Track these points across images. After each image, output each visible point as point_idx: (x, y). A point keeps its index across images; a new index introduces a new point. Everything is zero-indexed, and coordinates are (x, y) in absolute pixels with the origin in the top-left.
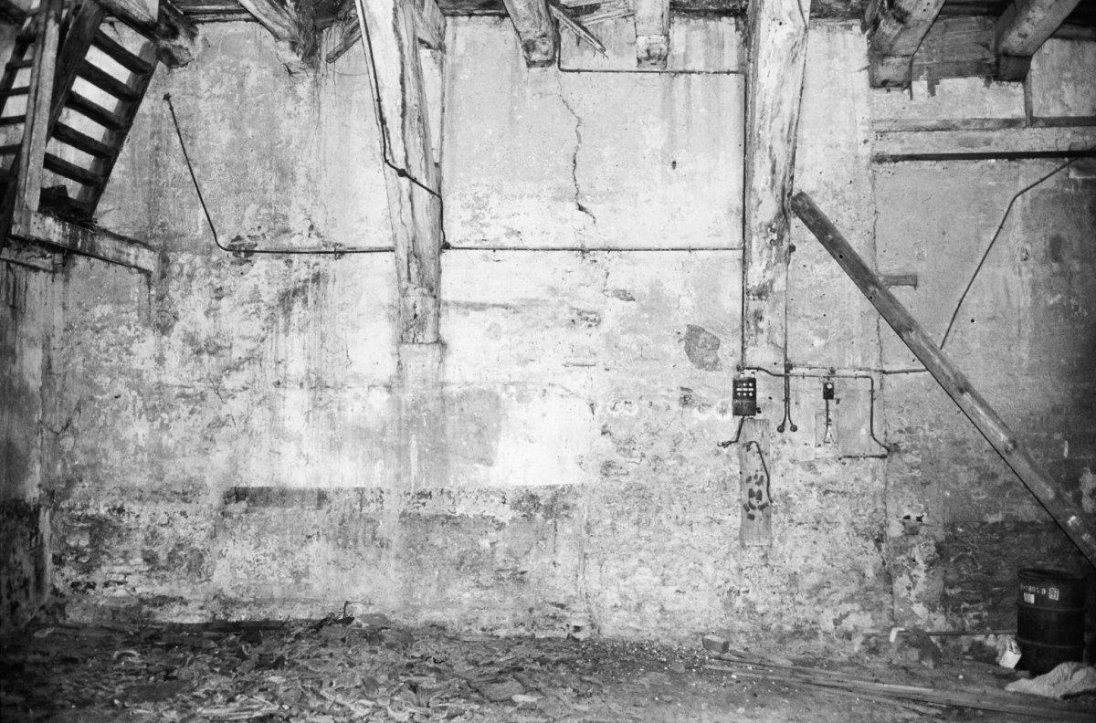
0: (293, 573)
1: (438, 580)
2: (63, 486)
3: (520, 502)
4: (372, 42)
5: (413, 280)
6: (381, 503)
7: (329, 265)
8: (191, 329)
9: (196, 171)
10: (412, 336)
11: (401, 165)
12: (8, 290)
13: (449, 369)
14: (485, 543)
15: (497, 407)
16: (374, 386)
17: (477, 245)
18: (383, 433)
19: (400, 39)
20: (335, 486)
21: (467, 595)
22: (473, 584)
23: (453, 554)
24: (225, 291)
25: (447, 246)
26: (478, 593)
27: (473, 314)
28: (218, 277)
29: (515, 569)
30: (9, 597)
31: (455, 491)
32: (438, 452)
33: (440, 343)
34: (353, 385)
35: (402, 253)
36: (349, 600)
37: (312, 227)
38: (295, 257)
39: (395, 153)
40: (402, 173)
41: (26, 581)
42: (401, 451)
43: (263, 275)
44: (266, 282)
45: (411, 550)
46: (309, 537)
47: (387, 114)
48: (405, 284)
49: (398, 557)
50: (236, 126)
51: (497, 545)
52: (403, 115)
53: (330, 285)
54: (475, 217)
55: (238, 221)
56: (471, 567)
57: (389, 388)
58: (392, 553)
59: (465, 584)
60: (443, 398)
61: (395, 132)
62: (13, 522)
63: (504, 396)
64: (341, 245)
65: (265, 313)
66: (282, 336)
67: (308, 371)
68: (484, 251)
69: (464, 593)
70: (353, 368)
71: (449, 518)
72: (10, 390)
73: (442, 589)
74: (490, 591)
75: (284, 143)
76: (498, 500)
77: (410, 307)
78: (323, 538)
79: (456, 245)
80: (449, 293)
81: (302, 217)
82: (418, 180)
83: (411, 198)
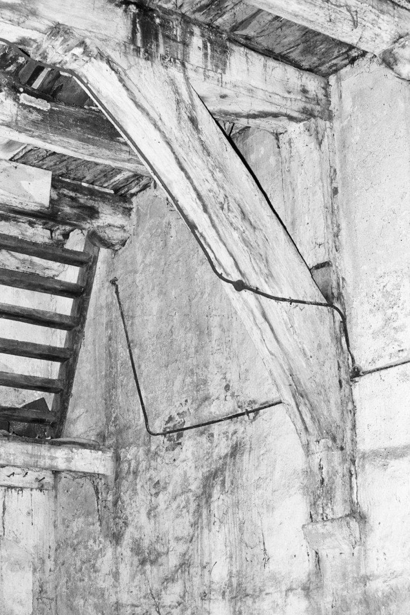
5: (310, 430)
7: (245, 429)
8: (137, 536)
9: (136, 351)
10: (321, 511)
11: (236, 277)
13: (372, 555)
16: (290, 589)
19: (148, 114)
24: (162, 484)
25: (356, 373)
28: (155, 469)
33: (356, 514)
34: (271, 590)
35: (288, 398)
37: (227, 388)
38: (215, 429)
40: (240, 286)
44: (193, 467)
47: (192, 217)
48: (304, 437)
50: (163, 293)
52: (205, 210)
53: (246, 457)
54: (388, 320)
57: (307, 590)
64: (254, 402)
65: (193, 506)
67: (230, 575)
70: (272, 566)
75: (199, 295)
77: (316, 469)
81: (220, 376)
82: (261, 290)
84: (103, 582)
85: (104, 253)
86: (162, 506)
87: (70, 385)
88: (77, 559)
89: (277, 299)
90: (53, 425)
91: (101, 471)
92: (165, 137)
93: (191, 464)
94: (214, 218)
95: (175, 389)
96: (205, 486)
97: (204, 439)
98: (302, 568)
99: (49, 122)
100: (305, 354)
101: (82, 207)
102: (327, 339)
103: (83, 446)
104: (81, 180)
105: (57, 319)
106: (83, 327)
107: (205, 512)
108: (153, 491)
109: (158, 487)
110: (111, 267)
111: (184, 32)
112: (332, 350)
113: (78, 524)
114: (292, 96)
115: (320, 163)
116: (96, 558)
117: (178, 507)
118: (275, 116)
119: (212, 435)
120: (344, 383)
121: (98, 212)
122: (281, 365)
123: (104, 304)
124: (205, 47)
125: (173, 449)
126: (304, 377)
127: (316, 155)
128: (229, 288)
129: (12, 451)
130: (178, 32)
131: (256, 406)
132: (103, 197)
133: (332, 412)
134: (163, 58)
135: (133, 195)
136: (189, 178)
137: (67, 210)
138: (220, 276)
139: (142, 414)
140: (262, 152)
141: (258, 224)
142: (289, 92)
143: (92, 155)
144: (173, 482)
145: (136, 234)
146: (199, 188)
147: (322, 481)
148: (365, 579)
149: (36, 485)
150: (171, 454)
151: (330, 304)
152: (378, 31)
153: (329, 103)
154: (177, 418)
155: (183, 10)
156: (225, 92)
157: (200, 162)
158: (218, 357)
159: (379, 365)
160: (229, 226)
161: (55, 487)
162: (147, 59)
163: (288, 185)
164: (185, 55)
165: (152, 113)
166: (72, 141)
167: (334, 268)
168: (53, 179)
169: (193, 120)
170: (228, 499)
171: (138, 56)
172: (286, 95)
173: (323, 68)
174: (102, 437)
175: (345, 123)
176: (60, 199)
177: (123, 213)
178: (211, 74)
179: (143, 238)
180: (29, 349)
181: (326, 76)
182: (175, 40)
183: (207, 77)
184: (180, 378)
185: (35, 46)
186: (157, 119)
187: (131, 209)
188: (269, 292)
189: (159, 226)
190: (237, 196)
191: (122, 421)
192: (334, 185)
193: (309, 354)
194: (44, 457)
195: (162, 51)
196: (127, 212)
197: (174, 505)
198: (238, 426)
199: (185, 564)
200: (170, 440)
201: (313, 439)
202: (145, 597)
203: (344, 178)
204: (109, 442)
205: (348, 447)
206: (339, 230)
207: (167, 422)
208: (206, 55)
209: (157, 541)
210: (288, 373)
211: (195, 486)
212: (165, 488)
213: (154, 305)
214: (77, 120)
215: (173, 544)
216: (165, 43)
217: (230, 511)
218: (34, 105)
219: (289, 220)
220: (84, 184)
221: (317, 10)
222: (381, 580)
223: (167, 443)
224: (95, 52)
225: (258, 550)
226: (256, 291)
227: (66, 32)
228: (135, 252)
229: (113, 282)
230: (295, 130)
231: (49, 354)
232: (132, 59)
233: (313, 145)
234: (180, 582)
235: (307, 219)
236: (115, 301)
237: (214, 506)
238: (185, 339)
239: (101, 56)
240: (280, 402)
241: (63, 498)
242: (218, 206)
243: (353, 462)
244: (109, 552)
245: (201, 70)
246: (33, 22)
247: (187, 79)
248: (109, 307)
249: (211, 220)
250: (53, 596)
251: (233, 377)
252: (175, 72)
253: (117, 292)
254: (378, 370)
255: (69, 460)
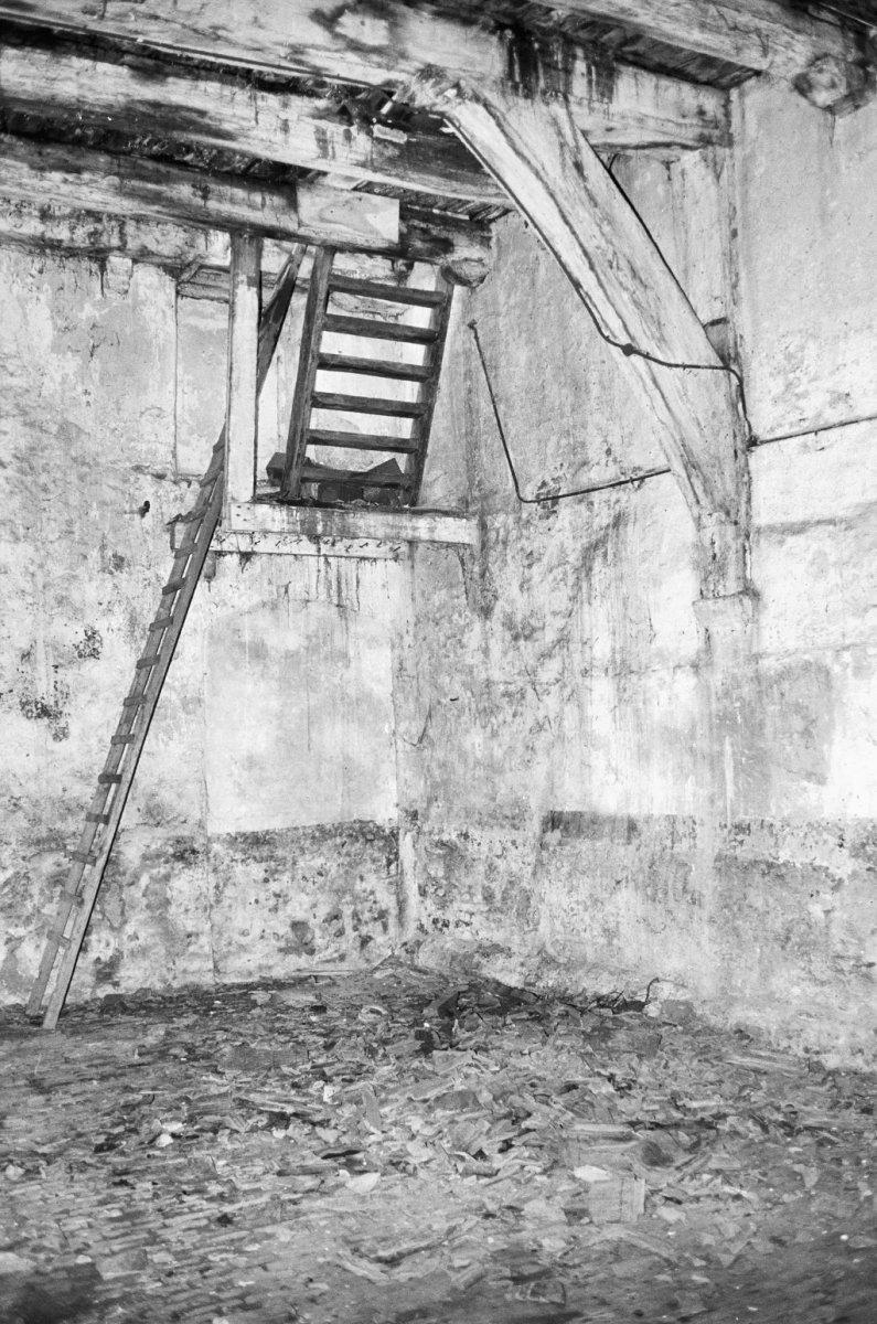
0: (605, 930)
1: (760, 962)
2: (425, 805)
3: (863, 845)
4: (506, 180)
6: (694, 838)
7: (629, 498)
8: (508, 609)
9: (502, 408)
11: (624, 340)
12: (329, 588)
13: (766, 633)
14: (816, 910)
15: (829, 686)
16: (679, 666)
17: (796, 430)
18: (692, 736)
19: (529, 163)
20: (645, 812)
21: (796, 991)
22: (803, 974)
23: (777, 924)
24: (535, 555)
25: (753, 442)
26: (812, 990)
27: (791, 540)
28: (528, 538)
29: (858, 958)
30: (355, 929)
31: (778, 825)
32: (756, 764)
33: (750, 591)
35: (677, 467)
36: (660, 976)
37: (609, 452)
38: (595, 496)
39: (611, 325)
40: (628, 350)
41: (382, 915)
42: (714, 761)
43: (566, 530)
45: (726, 911)
46: (618, 882)
47: (576, 274)
48: (696, 510)
49: (712, 921)
50: (532, 341)
51: (832, 915)
52: (592, 268)
53: (630, 528)
54: (789, 386)
55: (541, 467)
56: (800, 946)
57: (695, 667)
58: (705, 916)
59: (794, 972)
60: (758, 678)
61: (597, 295)
62: (358, 845)
63: (836, 669)
64: (639, 469)
65: (571, 579)
66: (586, 605)
67: (613, 650)
68: (802, 438)
69: (792, 984)
70: (658, 643)
71: (770, 866)
72: (343, 699)
73: (765, 976)
74: (826, 989)
76: (834, 841)
77: (707, 543)
78: (631, 884)
79: (769, 437)
80: (763, 514)
82: (651, 355)
83: (655, 381)
84: (472, 658)
85: (458, 290)
86: (536, 579)
87: (424, 445)
88: (441, 634)
89: (670, 365)
90: (407, 490)
91: (467, 540)
92: (547, 188)
93: (568, 534)
94: (602, 277)
95: (549, 452)
96: (584, 558)
97: (583, 507)
98: (692, 646)
99: (409, 157)
100: (699, 424)
101: (435, 240)
102: (723, 405)
103: (446, 514)
104: (432, 206)
105: (409, 371)
106: (437, 378)
107: (585, 585)
108: (526, 562)
109: (531, 558)
110: (468, 307)
111: (565, 60)
112: (728, 417)
113: (440, 597)
114: (687, 121)
115: (719, 202)
116: (463, 633)
117: (555, 579)
118: (668, 145)
119: (592, 503)
120: (739, 452)
121: (452, 245)
122: (672, 435)
123: (461, 351)
124: (589, 72)
125: (548, 518)
126: (697, 447)
127: (713, 191)
128: (616, 351)
129: (372, 523)
130: (559, 57)
131: (641, 474)
132: (456, 225)
133: (726, 485)
134: (544, 93)
135: (494, 220)
136: (574, 233)
137: (419, 244)
138: (607, 339)
139: (511, 478)
140: (649, 179)
141: (650, 282)
142: (684, 117)
143: (454, 191)
144: (548, 553)
145: (497, 269)
146: (586, 245)
147: (714, 557)
148: (756, 658)
149: (390, 555)
150: (546, 523)
151: (726, 367)
152: (791, 54)
153: (729, 123)
154: (551, 483)
155: (564, 29)
156: (611, 124)
157: (587, 215)
158: (597, 417)
159: (779, 434)
160: (617, 286)
161: (411, 557)
162: (526, 97)
163: (679, 224)
164: (568, 85)
165: (533, 162)
166: (434, 179)
167: (731, 325)
168: (401, 208)
169: (578, 166)
170: (611, 572)
171: (517, 95)
172: (681, 121)
173: (724, 81)
174: (465, 502)
175: (748, 151)
176: (409, 233)
177: (482, 243)
178: (596, 105)
179: (506, 273)
180: (381, 406)
181: (725, 89)
182: (556, 68)
183: (592, 110)
184: (554, 439)
185: (401, 87)
186: (540, 168)
187: (490, 238)
188: (661, 358)
189: (523, 262)
190: (627, 251)
191: (487, 486)
192: (733, 226)
193: (703, 424)
194: (405, 527)
195: (542, 84)
196: (485, 242)
197: (551, 577)
198: (621, 494)
199: (563, 640)
200: (544, 507)
201: (705, 513)
202: (519, 674)
203: (744, 219)
204: (472, 508)
205: (743, 521)
206: (737, 281)
207: (540, 488)
208: (590, 82)
209: (531, 615)
210: (680, 443)
211: (574, 558)
212: (539, 560)
213: (522, 355)
214: (437, 151)
215: (549, 618)
216: (545, 73)
217: (613, 584)
218: (389, 138)
219: (681, 267)
220: (436, 211)
221: (722, 38)
222: (772, 658)
223: (541, 511)
224: (471, 93)
225: (644, 626)
226: (647, 356)
227: (437, 74)
228: (497, 291)
229: (472, 326)
230: (690, 159)
231: (401, 410)
232: (511, 99)
233: (710, 179)
234: (559, 658)
235: (701, 266)
236: (474, 348)
237: (595, 580)
238: (558, 395)
239: (477, 98)
240: (668, 471)
241: (420, 568)
242: (606, 264)
243: (748, 537)
244: (477, 626)
245: (585, 102)
246: (403, 65)
247: (570, 114)
248: (467, 354)
249: (598, 279)
250: (415, 673)
251: (615, 440)
252: (557, 109)
253: (476, 338)
254: (777, 439)
255: (432, 530)
